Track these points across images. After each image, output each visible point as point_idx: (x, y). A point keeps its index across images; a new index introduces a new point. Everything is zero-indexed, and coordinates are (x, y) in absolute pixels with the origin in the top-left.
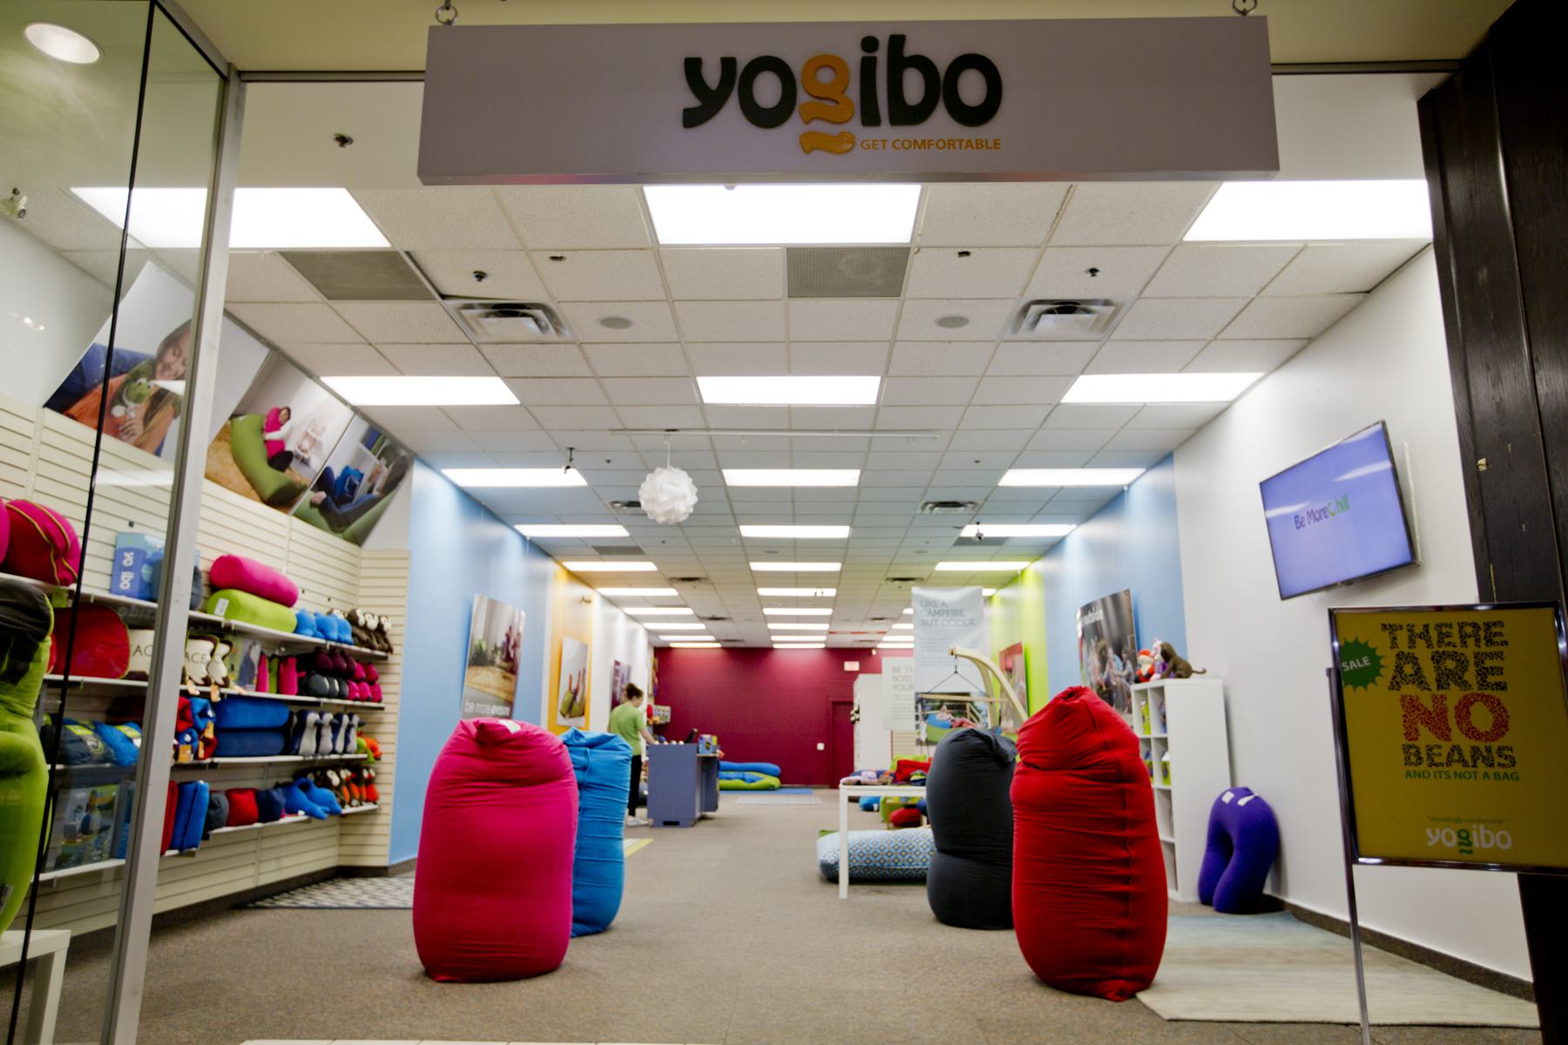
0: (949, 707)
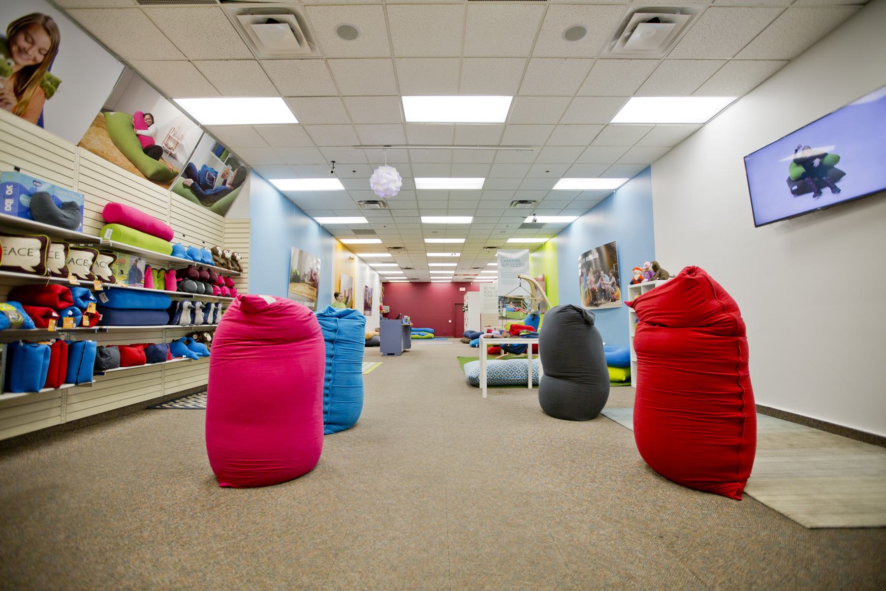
0: (513, 303)
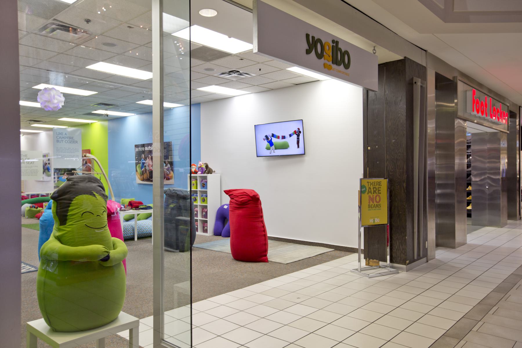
0: (67, 174)
